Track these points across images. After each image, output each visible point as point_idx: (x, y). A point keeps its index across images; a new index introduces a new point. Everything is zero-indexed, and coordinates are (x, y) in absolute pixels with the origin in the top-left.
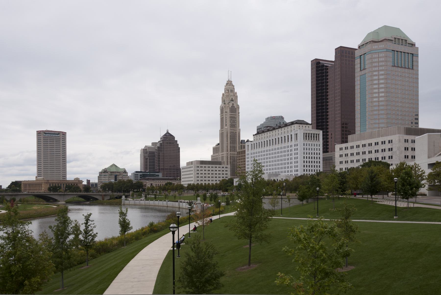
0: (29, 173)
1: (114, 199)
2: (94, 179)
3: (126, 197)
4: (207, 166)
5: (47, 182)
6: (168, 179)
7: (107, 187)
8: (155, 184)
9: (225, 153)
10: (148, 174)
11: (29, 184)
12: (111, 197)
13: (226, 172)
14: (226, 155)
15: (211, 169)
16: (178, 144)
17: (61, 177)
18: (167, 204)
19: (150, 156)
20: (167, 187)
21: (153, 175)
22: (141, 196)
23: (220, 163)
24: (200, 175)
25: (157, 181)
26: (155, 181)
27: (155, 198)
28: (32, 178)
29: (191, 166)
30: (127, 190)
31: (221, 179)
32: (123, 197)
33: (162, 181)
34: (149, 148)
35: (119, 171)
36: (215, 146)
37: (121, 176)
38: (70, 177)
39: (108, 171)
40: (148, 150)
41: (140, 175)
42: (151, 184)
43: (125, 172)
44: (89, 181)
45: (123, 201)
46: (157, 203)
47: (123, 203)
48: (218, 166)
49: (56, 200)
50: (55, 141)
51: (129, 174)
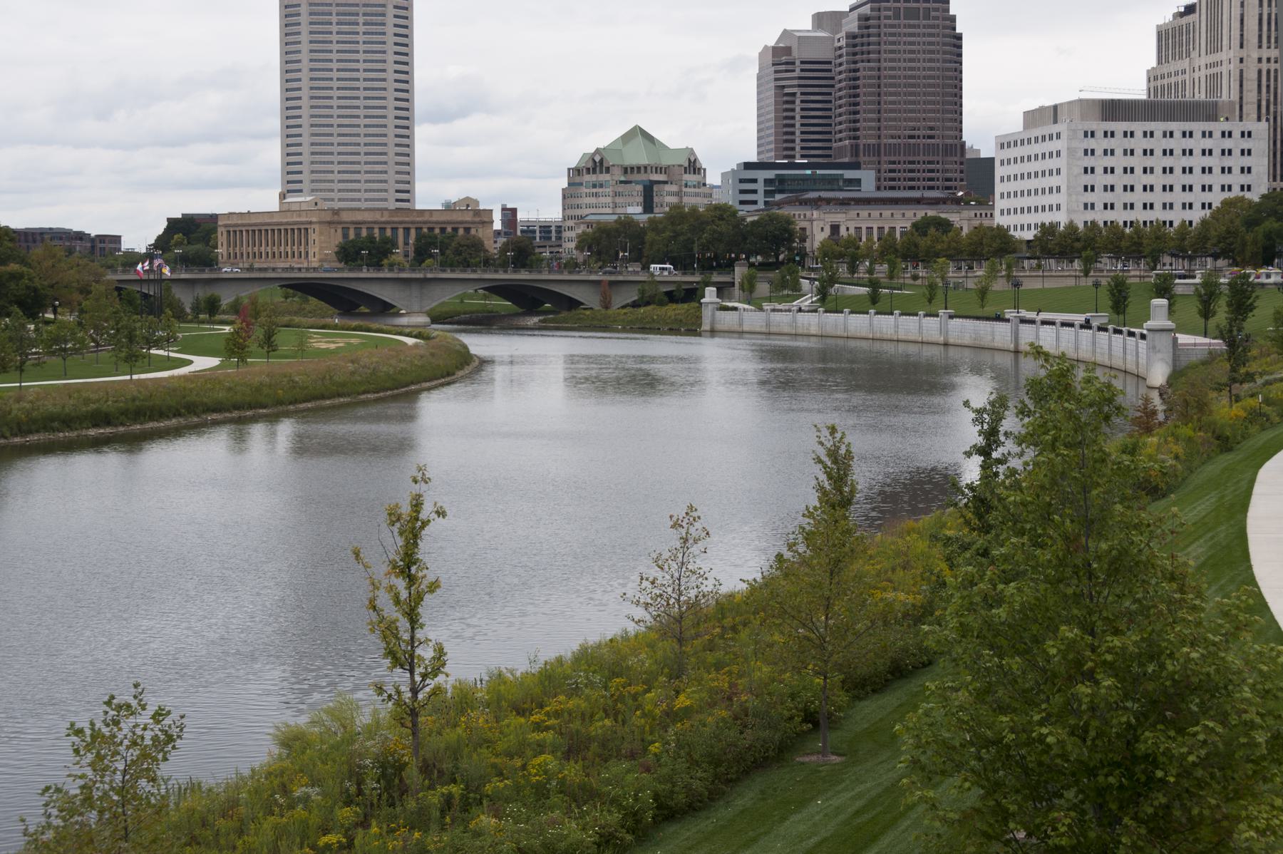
0: (245, 180)
1: (661, 304)
2: (542, 205)
3: (722, 290)
4: (1138, 127)
5: (333, 220)
6: (918, 201)
7: (607, 243)
8: (852, 225)
9: (1228, 54)
10: (805, 179)
11: (252, 229)
12: (642, 292)
13: (1246, 161)
14: (1234, 67)
15: (1177, 144)
16: (953, 19)
17: (392, 196)
18: (943, 330)
19: (803, 85)
20: (924, 242)
21: (831, 183)
22: (796, 288)
23: (1208, 112)
24: (1100, 179)
25: (864, 214)
26: (853, 213)
27: (874, 299)
28: (263, 199)
29: (1054, 129)
30: (716, 257)
31: (1216, 198)
32: (710, 295)
33: (887, 213)
34: (803, 40)
35: (665, 161)
36: (1169, 17)
37: (674, 188)
38: (431, 194)
39: (611, 160)
40: (795, 54)
41: (767, 182)
42: (835, 228)
43: (693, 166)
44: (514, 211)
45: (707, 313)
46: (886, 324)
47: (706, 326)
48: (1197, 127)
49: (385, 309)
50: (361, 19)
51: (713, 178)
